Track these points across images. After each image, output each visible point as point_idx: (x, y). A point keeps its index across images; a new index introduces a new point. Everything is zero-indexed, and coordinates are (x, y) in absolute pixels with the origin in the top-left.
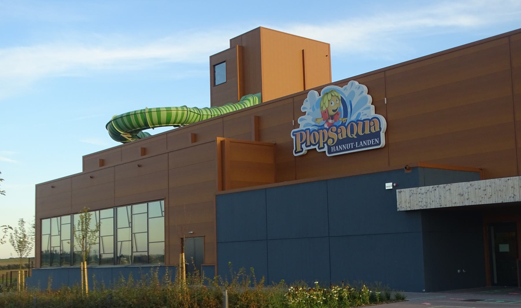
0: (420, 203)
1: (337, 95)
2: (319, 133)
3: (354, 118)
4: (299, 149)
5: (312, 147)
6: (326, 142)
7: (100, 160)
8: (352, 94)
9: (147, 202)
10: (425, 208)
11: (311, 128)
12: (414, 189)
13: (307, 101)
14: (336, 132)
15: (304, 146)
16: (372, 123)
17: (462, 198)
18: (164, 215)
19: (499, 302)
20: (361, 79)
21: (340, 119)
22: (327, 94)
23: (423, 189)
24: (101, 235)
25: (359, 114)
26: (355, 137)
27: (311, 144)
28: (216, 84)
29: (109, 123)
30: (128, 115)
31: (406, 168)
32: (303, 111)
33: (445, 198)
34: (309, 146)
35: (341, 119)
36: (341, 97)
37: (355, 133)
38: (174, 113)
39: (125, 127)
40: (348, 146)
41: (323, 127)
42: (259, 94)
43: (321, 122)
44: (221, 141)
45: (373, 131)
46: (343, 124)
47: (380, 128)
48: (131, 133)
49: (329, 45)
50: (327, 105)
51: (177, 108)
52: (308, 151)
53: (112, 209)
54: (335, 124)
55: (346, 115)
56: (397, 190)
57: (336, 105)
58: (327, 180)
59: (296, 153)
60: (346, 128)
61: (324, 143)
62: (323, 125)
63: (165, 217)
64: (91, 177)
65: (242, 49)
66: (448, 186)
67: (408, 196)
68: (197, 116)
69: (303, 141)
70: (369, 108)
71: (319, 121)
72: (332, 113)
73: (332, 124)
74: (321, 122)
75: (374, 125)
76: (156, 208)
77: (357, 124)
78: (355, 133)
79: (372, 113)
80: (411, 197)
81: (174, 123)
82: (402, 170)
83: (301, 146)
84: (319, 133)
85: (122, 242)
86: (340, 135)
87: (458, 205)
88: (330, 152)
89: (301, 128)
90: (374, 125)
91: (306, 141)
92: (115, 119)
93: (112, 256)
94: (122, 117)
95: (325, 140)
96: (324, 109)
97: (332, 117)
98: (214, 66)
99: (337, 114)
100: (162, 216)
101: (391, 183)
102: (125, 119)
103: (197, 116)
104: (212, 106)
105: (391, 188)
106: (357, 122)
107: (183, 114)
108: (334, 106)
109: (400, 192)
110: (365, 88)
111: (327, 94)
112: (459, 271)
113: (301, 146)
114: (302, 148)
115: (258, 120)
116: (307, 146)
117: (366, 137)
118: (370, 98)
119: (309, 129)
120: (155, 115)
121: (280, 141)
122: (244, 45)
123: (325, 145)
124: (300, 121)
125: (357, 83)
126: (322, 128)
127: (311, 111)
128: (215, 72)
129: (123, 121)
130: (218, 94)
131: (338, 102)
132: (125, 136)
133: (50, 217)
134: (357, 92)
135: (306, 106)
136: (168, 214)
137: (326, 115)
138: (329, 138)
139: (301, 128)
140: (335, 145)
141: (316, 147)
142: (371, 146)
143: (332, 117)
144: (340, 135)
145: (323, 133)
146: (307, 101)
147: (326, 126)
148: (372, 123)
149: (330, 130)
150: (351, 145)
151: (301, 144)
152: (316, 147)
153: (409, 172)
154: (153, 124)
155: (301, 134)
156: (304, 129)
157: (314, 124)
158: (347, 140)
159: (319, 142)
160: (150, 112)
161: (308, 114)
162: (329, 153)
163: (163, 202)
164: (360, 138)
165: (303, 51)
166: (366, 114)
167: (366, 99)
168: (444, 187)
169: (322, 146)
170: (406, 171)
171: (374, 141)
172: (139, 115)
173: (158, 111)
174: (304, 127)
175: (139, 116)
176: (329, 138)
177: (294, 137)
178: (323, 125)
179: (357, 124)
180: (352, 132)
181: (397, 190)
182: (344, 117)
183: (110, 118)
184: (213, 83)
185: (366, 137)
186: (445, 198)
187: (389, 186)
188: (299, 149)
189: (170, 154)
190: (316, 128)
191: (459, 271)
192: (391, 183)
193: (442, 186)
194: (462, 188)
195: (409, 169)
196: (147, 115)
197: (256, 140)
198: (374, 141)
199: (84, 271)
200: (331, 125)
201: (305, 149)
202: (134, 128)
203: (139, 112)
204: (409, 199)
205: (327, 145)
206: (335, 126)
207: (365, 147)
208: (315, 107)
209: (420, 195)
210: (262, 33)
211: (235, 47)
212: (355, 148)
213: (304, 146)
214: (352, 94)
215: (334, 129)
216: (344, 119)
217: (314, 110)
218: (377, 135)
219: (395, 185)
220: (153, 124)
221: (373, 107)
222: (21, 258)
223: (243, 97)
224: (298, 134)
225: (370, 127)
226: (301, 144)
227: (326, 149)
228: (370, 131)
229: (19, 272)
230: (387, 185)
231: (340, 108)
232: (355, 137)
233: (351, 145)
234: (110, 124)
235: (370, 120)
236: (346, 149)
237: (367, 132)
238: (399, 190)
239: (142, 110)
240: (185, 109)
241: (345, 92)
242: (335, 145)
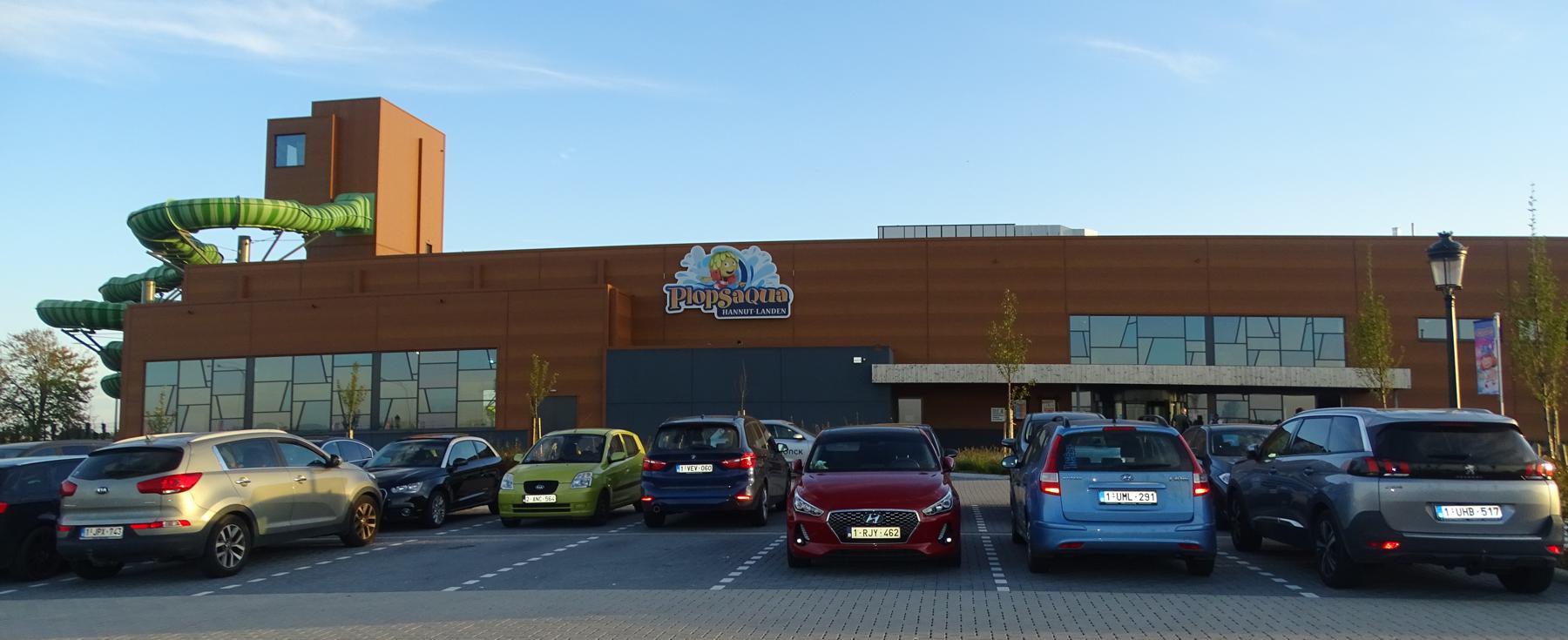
3: (755, 284)
4: (675, 306)
8: (755, 260)
20: (764, 246)
40: (745, 311)
55: (744, 279)
65: (339, 121)
74: (711, 282)
79: (776, 283)
88: (720, 314)
97: (726, 279)
108: (729, 267)
115: (247, 280)
120: (198, 210)
126: (711, 288)
135: (687, 261)
137: (716, 275)
143: (726, 279)
158: (744, 305)
164: (761, 306)
173: (220, 203)
180: (752, 297)
187: (857, 360)
188: (675, 306)
200: (723, 287)
210: (383, 104)
218: (785, 305)
222: (250, 358)
223: (342, 196)
227: (715, 310)
237: (772, 300)
241: (746, 256)
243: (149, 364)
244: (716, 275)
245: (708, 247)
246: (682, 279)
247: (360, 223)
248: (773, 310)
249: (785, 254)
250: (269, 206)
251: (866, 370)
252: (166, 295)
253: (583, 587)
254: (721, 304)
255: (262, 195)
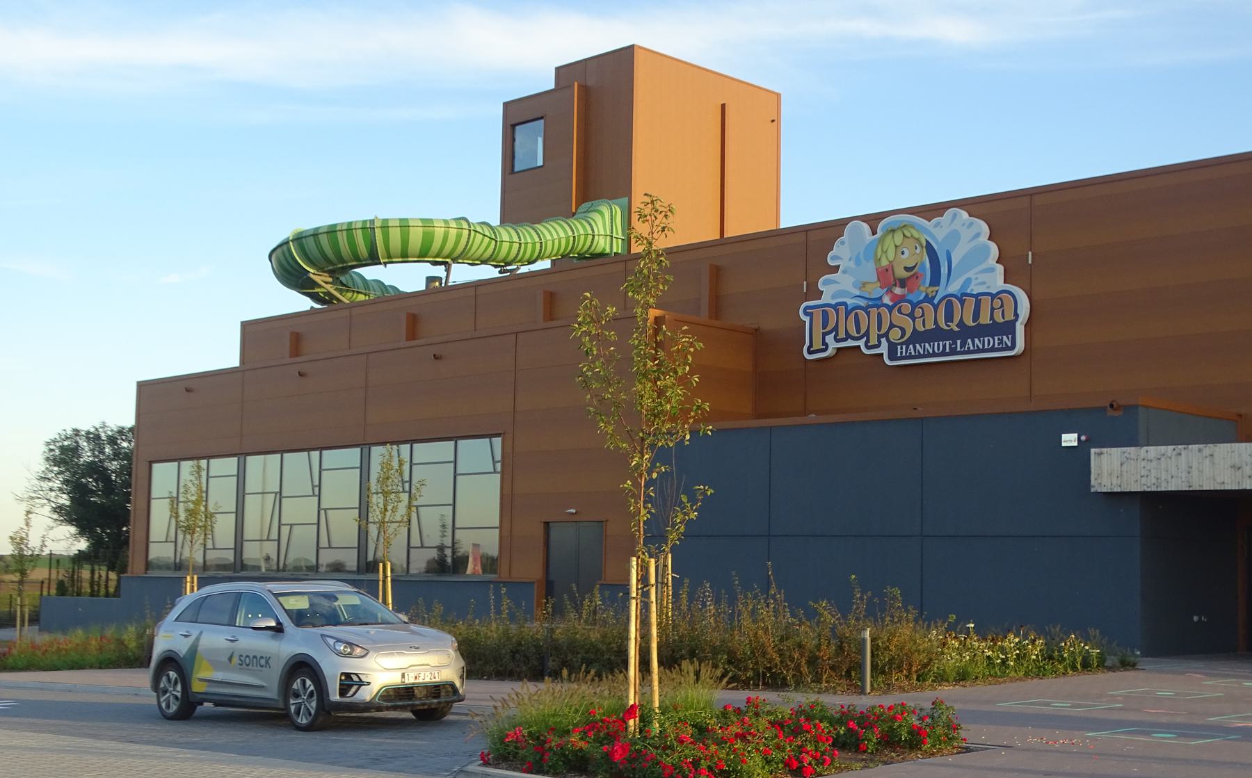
0: (1144, 480)
1: (916, 235)
2: (868, 314)
3: (954, 288)
4: (818, 345)
5: (850, 343)
6: (886, 335)
7: (292, 334)
8: (954, 237)
9: (456, 438)
10: (1153, 489)
11: (850, 302)
12: (1132, 450)
13: (843, 243)
14: (912, 316)
15: (830, 339)
16: (997, 303)
17: (1239, 473)
18: (499, 469)
19: (276, 772)
20: (974, 206)
21: (922, 288)
22: (893, 231)
23: (1153, 451)
24: (323, 506)
25: (968, 281)
26: (956, 329)
27: (849, 336)
28: (516, 169)
29: (280, 246)
30: (332, 231)
31: (1112, 406)
32: (831, 263)
33: (1201, 471)
34: (844, 340)
35: (924, 288)
36: (927, 242)
37: (956, 320)
38: (439, 232)
39: (311, 260)
40: (937, 346)
41: (879, 303)
42: (626, 199)
43: (876, 291)
44: (656, 318)
45: (999, 319)
46: (929, 299)
47: (1016, 315)
48: (331, 273)
49: (778, 96)
50: (891, 256)
51: (446, 221)
52: (839, 349)
53: (359, 450)
54: (909, 297)
55: (935, 281)
56: (1093, 450)
57: (913, 256)
58: (922, 419)
59: (810, 352)
60: (936, 308)
61: (880, 337)
62: (880, 298)
63: (503, 473)
64: (301, 374)
65: (585, 91)
66: (1208, 449)
67: (1116, 463)
68: (489, 244)
69: (828, 329)
70: (992, 270)
71: (869, 288)
72: (901, 273)
73: (904, 296)
74: (876, 291)
75: (1002, 306)
76: (479, 454)
77: (962, 302)
78: (956, 320)
79: (996, 281)
80: (1125, 467)
81: (437, 256)
82: (1104, 409)
83: (824, 339)
84: (868, 314)
85: (291, 525)
86: (919, 322)
87: (1228, 487)
88: (893, 356)
89: (825, 299)
90: (1002, 306)
91: (836, 329)
92: (299, 239)
93: (230, 556)
94: (315, 234)
95: (883, 331)
96: (884, 263)
97: (903, 283)
98: (514, 126)
99: (916, 276)
100: (495, 472)
101: (1076, 435)
102: (324, 240)
103: (489, 244)
104: (504, 220)
105: (1076, 444)
106: (962, 297)
107: (459, 237)
108: (908, 259)
109: (1100, 454)
110: (985, 228)
111: (893, 231)
112: (1196, 618)
113: (824, 339)
114: (825, 344)
115: (717, 273)
116: (837, 340)
117: (981, 331)
118: (994, 249)
119: (845, 304)
120: (395, 236)
121: (769, 323)
122: (591, 82)
123: (883, 340)
124: (824, 283)
125: (965, 215)
126: (877, 303)
127: (852, 264)
128: (514, 140)
129: (318, 244)
130: (524, 197)
131: (918, 251)
132: (317, 279)
133: (178, 460)
134: (966, 234)
135: (840, 253)
136: (510, 469)
137: (886, 276)
138: (892, 326)
139: (825, 299)
140: (907, 343)
141: (861, 343)
142: (993, 349)
143: (903, 283)
144: (919, 322)
145: (879, 314)
146: (843, 243)
147: (887, 300)
148: (997, 303)
149: (895, 311)
150: (944, 346)
151: (824, 335)
152: (861, 343)
153: (1116, 414)
154: (389, 257)
155: (825, 314)
156: (833, 302)
157: (858, 293)
158: (936, 334)
159: (867, 334)
160: (385, 227)
161: (845, 272)
162: (891, 359)
163: (497, 441)
164: (966, 332)
165: (723, 106)
166: (984, 283)
167: (987, 250)
168: (1200, 450)
169: (874, 341)
170: (1110, 413)
171: (1001, 341)
172: (359, 232)
173: (404, 225)
174: (833, 297)
175: (359, 237)
176: (892, 326)
177: (807, 319)
178: (880, 298)
179: (962, 302)
180: (949, 317)
181: (1093, 450)
182: (931, 284)
183: (287, 233)
184: (509, 164)
185: (981, 331)
186: (1201, 471)
187: (1070, 439)
188: (818, 345)
189: (520, 336)
190: (863, 303)
191: (1196, 618)
192: (1076, 435)
193: (1195, 447)
194: (1240, 455)
195: (1119, 408)
196: (378, 234)
197: (710, 317)
198: (1001, 341)
199: (384, 582)
201: (833, 345)
202: (343, 261)
203: (360, 226)
204: (1117, 469)
205: (888, 340)
206: (909, 302)
207: (979, 351)
208: (862, 257)
209: (1143, 463)
211: (571, 86)
212: (953, 352)
213: (830, 339)
214: (954, 237)
215: (907, 308)
216: (931, 289)
217: (858, 262)
218: (1009, 328)
219: (1083, 438)
220: (389, 257)
221: (1000, 268)
223: (585, 206)
224: (818, 314)
225: (993, 309)
226: (824, 335)
227: (884, 349)
228: (992, 318)
229: (189, 579)
230: (1065, 437)
231: (923, 264)
232: (956, 329)
233: (944, 346)
234: (285, 247)
235: (993, 296)
236: (932, 353)
237: (985, 319)
238: (1097, 450)
239: (365, 222)
240: (465, 225)
241: (937, 231)
242: (907, 343)
243: (156, 466)
244: (886, 276)
245: (873, 220)
246: (833, 289)
247: (602, 244)
248: (988, 341)
249: (1023, 220)
250: (505, 235)
251: (1080, 455)
252: (673, 537)
253: (248, 754)
254: (895, 335)
255: (495, 220)
